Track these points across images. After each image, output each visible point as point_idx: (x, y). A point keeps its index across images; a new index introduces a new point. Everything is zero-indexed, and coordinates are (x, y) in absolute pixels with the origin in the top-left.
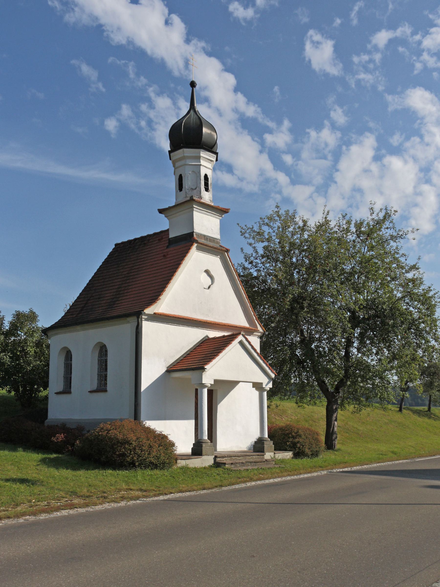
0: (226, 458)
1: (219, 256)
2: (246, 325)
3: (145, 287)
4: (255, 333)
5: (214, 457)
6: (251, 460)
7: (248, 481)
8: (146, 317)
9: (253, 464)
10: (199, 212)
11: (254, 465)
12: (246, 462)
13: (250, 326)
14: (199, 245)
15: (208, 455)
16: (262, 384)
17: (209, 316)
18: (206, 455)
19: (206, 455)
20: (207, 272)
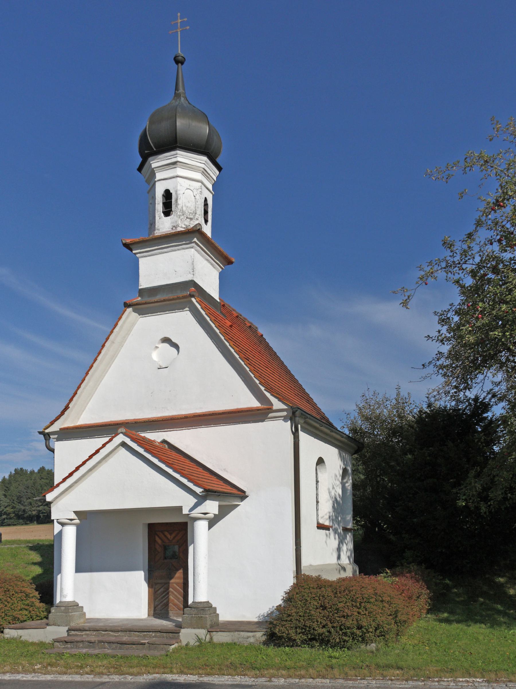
0: (88, 632)
1: (187, 309)
2: (254, 403)
3: (275, 374)
4: (271, 415)
5: (66, 628)
6: (113, 639)
7: (254, 685)
8: (56, 436)
9: (114, 646)
10: (149, 256)
11: (116, 647)
12: (100, 642)
13: (262, 405)
14: (134, 307)
15: (59, 626)
16: (180, 508)
17: (168, 410)
18: (54, 625)
19: (55, 625)
20: (166, 340)
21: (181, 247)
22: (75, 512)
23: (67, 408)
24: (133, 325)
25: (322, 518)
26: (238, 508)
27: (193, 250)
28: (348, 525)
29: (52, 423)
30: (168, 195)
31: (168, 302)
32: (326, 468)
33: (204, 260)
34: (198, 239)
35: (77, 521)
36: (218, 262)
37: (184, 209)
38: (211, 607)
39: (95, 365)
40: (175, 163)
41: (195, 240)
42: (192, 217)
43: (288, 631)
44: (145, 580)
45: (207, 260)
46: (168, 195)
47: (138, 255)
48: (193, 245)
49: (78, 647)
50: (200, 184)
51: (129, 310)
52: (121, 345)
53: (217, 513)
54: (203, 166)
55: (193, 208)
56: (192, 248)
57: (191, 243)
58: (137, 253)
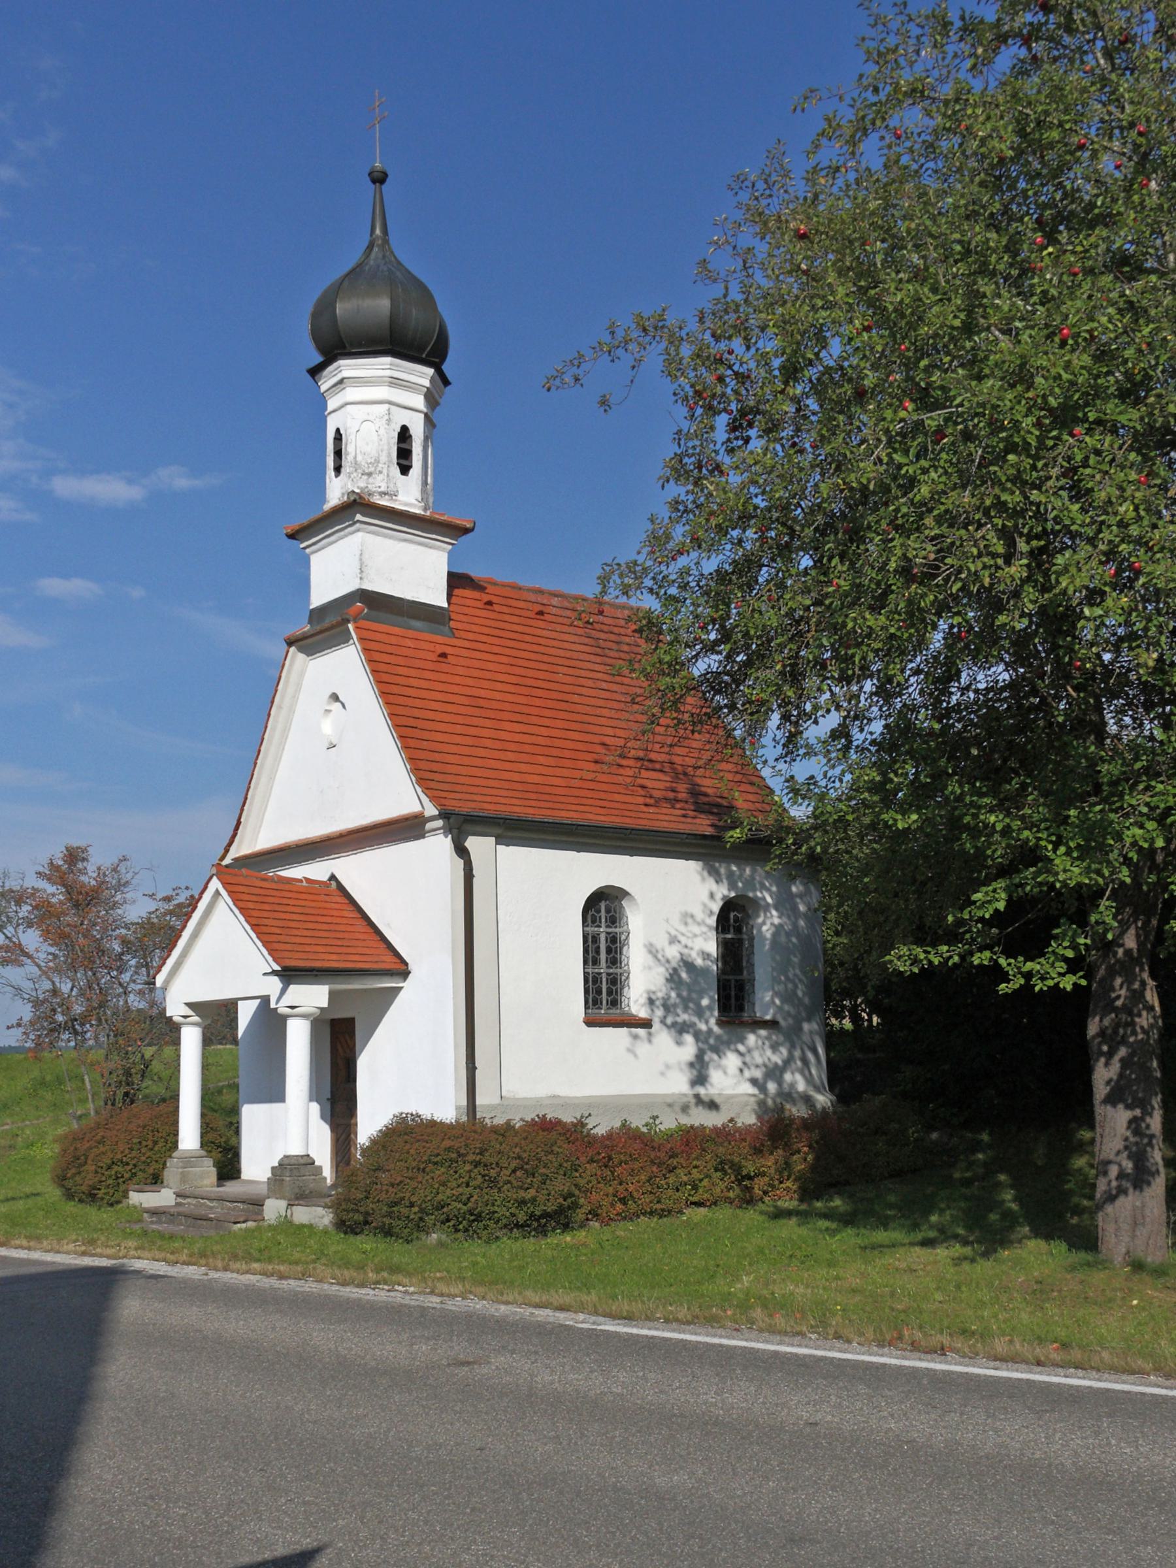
10: (319, 550)
21: (347, 531)
22: (189, 1005)
23: (239, 823)
24: (302, 674)
25: (636, 1001)
26: (402, 994)
27: (360, 534)
28: (767, 1014)
29: (227, 851)
30: (338, 436)
31: (327, 634)
32: (637, 904)
33: (396, 542)
34: (364, 515)
35: (196, 1019)
36: (434, 536)
37: (359, 458)
38: (313, 1163)
39: (263, 749)
40: (341, 381)
41: (359, 517)
42: (372, 469)
43: (358, 1211)
44: (323, 1117)
45: (405, 540)
46: (338, 436)
47: (308, 551)
48: (358, 525)
49: (159, 1222)
50: (386, 406)
51: (293, 649)
52: (292, 711)
53: (325, 1004)
54: (388, 373)
55: (374, 453)
56: (358, 530)
57: (355, 523)
58: (305, 548)
